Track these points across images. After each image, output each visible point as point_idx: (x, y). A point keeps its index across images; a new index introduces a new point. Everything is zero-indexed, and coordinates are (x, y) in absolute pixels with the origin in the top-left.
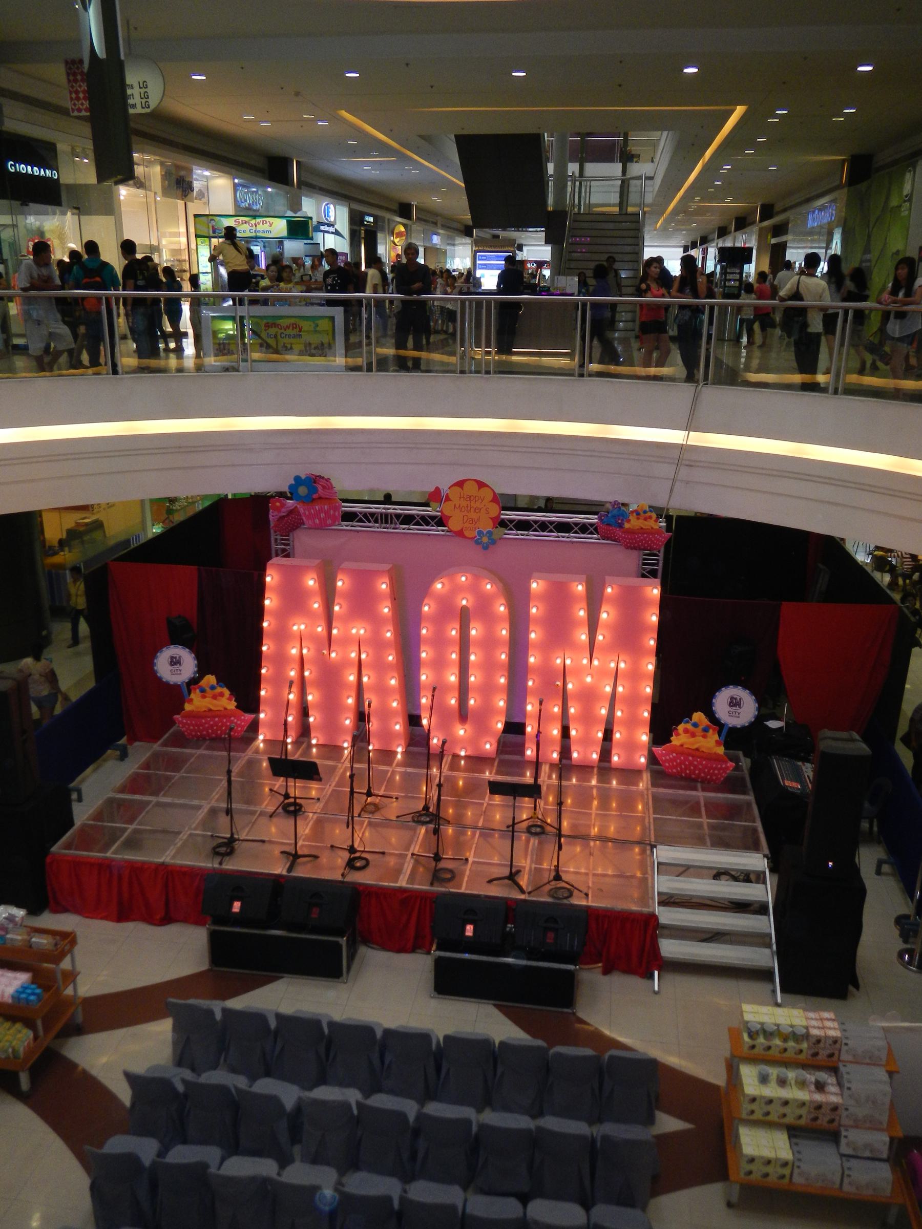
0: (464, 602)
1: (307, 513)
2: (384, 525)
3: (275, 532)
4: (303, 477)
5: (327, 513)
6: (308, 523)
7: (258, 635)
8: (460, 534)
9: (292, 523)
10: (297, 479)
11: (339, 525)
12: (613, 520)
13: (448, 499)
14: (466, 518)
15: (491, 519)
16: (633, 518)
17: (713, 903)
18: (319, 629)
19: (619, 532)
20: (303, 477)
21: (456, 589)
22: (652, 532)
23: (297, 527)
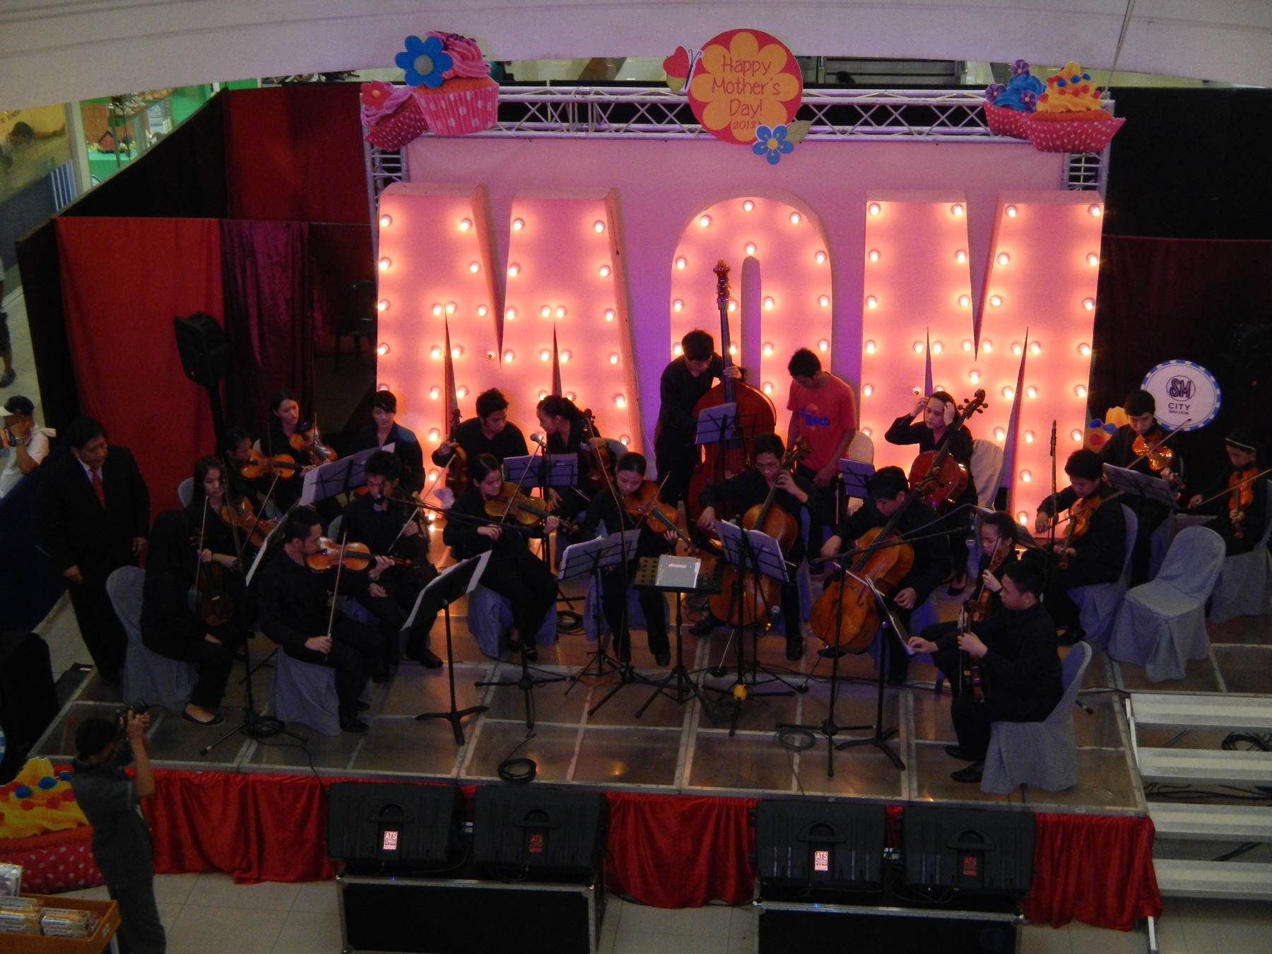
0: (751, 251)
1: (432, 107)
2: (579, 125)
3: (372, 147)
4: (423, 39)
5: (470, 106)
6: (435, 126)
7: (368, 329)
8: (725, 135)
9: (404, 126)
10: (412, 42)
11: (493, 128)
12: (1014, 98)
13: (701, 69)
14: (735, 105)
15: (784, 104)
16: (1052, 92)
17: (1227, 792)
18: (482, 312)
19: (1025, 119)
20: (423, 39)
21: (735, 227)
22: (1089, 117)
23: (416, 135)
